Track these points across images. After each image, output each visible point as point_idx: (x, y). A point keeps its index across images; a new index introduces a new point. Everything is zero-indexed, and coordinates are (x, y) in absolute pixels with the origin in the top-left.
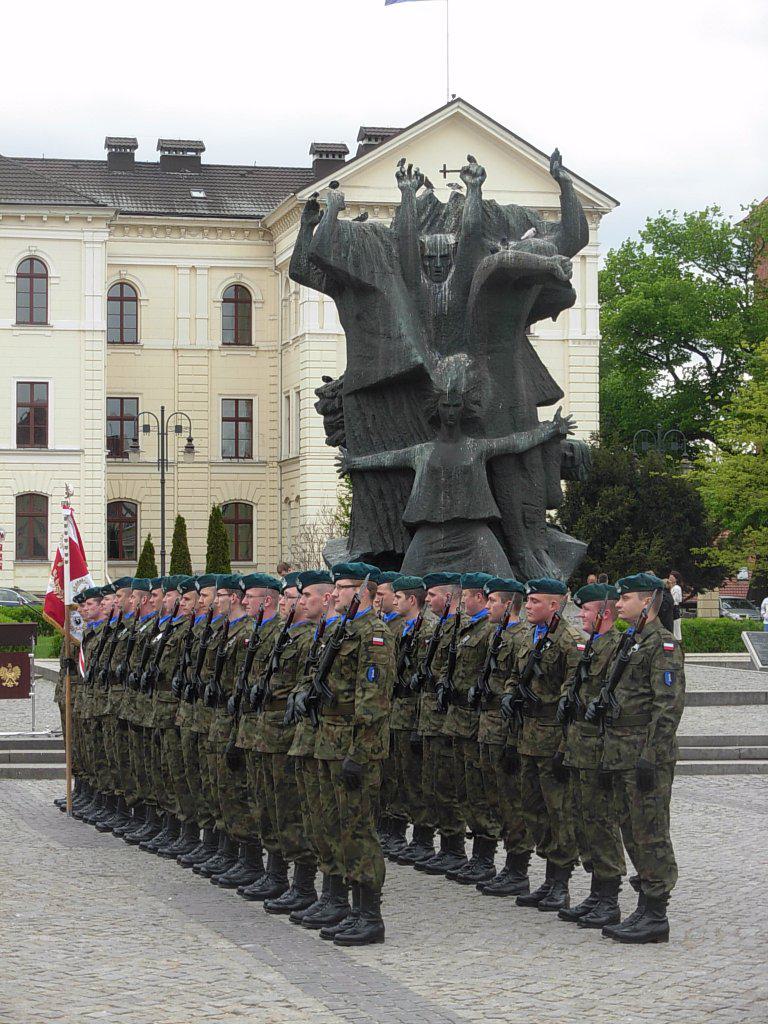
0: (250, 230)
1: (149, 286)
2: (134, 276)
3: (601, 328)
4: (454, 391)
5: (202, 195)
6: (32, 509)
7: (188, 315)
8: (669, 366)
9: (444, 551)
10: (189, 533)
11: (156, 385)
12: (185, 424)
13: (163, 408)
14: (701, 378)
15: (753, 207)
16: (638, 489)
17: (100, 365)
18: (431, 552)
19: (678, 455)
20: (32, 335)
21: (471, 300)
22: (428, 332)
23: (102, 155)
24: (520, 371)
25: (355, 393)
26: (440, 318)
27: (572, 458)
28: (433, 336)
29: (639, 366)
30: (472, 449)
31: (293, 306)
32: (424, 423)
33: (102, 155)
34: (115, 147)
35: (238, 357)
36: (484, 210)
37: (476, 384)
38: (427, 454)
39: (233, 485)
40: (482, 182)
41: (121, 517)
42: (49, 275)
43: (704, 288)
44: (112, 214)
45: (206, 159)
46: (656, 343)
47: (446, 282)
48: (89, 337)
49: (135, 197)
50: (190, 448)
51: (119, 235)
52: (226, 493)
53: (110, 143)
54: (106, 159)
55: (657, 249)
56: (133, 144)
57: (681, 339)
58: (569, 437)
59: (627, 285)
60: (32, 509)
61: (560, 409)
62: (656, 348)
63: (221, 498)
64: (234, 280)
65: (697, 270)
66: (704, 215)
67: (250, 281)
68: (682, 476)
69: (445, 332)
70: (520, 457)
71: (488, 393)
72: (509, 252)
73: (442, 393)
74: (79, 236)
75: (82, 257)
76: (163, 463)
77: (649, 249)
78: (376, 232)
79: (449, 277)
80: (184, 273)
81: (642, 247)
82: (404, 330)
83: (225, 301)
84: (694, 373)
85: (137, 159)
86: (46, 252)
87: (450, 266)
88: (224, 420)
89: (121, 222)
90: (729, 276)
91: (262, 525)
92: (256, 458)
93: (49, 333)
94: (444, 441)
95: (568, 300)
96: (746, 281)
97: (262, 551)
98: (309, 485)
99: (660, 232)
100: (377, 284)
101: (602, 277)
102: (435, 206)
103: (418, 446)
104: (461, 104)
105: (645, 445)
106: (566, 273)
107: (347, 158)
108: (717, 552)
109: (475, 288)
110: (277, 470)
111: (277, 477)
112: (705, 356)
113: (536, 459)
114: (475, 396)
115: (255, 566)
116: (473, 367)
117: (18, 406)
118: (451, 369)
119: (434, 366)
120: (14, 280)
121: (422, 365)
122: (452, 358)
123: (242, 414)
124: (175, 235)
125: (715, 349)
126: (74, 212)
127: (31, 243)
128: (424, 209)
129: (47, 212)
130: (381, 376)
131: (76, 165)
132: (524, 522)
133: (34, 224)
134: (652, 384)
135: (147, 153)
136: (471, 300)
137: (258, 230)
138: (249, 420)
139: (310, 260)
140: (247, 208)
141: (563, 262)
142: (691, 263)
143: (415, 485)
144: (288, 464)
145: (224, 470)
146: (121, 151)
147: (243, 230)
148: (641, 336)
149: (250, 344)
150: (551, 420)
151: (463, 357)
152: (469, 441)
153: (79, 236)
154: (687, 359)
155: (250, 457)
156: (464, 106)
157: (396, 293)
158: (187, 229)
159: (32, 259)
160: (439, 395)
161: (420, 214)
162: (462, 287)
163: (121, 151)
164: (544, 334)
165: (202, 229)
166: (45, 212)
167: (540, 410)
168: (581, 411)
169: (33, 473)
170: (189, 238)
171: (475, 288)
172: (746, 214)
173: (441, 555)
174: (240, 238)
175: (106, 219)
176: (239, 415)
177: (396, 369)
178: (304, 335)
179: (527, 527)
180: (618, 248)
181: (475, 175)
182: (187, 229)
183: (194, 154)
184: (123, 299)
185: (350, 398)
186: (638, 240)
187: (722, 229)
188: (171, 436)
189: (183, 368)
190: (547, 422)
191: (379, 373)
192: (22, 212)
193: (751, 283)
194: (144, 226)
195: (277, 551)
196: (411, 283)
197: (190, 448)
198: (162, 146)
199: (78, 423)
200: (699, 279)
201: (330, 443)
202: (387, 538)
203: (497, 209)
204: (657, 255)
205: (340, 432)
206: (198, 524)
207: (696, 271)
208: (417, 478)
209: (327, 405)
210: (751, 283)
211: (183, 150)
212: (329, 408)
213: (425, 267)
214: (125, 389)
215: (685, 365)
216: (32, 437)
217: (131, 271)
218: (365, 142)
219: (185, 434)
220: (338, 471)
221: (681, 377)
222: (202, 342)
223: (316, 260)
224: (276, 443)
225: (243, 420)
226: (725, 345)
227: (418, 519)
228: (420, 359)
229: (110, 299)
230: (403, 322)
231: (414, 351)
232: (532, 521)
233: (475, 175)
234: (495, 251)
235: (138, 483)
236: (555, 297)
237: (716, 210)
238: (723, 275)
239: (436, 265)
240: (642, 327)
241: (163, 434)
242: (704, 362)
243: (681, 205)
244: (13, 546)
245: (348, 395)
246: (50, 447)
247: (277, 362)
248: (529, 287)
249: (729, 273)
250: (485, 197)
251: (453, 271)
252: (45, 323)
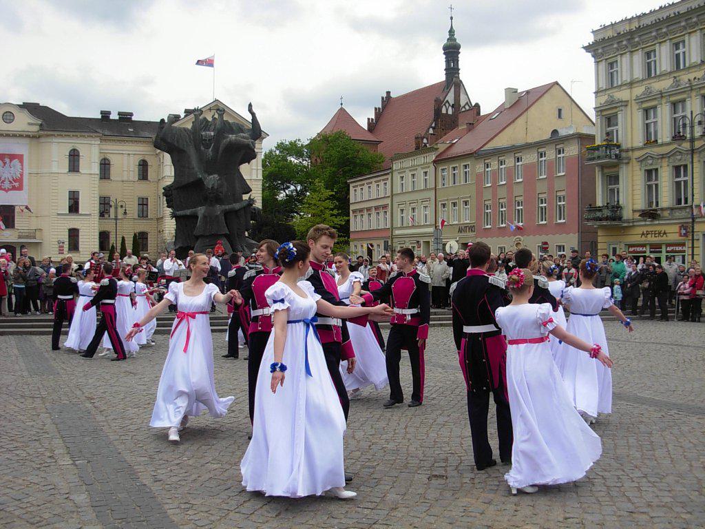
1: (115, 160)
2: (110, 157)
4: (212, 188)
10: (126, 242)
11: (114, 190)
12: (124, 205)
19: (288, 217)
21: (219, 155)
23: (100, 117)
24: (237, 182)
25: (177, 189)
30: (219, 209)
33: (100, 117)
35: (144, 184)
37: (221, 186)
39: (142, 226)
45: (134, 118)
48: (93, 176)
50: (125, 213)
56: (109, 113)
57: (287, 181)
63: (138, 230)
65: (293, 159)
66: (295, 142)
69: (209, 167)
70: (236, 212)
72: (232, 137)
73: (209, 188)
74: (89, 142)
76: (116, 219)
77: (278, 152)
80: (126, 157)
86: (79, 147)
89: (104, 139)
99: (281, 146)
100: (185, 149)
109: (220, 151)
118: (212, 180)
119: (206, 179)
123: (144, 203)
124: (123, 143)
133: (75, 138)
135: (114, 116)
136: (219, 155)
138: (147, 205)
139: (161, 140)
144: (160, 219)
148: (275, 180)
151: (216, 176)
153: (89, 142)
154: (289, 187)
157: (192, 152)
158: (127, 141)
159: (74, 150)
162: (216, 150)
164: (244, 169)
166: (78, 134)
167: (244, 195)
168: (256, 195)
169: (74, 222)
171: (220, 151)
176: (143, 203)
177: (192, 180)
182: (127, 141)
184: (105, 166)
186: (275, 149)
188: (119, 208)
189: (125, 186)
196: (197, 149)
197: (125, 213)
198: (119, 114)
199: (89, 204)
207: (293, 159)
222: (131, 179)
223: (163, 140)
230: (194, 162)
231: (198, 173)
235: (109, 226)
236: (249, 155)
237: (299, 140)
239: (207, 143)
240: (277, 173)
241: (116, 208)
243: (288, 138)
247: (156, 185)
249: (303, 160)
252: (78, 171)
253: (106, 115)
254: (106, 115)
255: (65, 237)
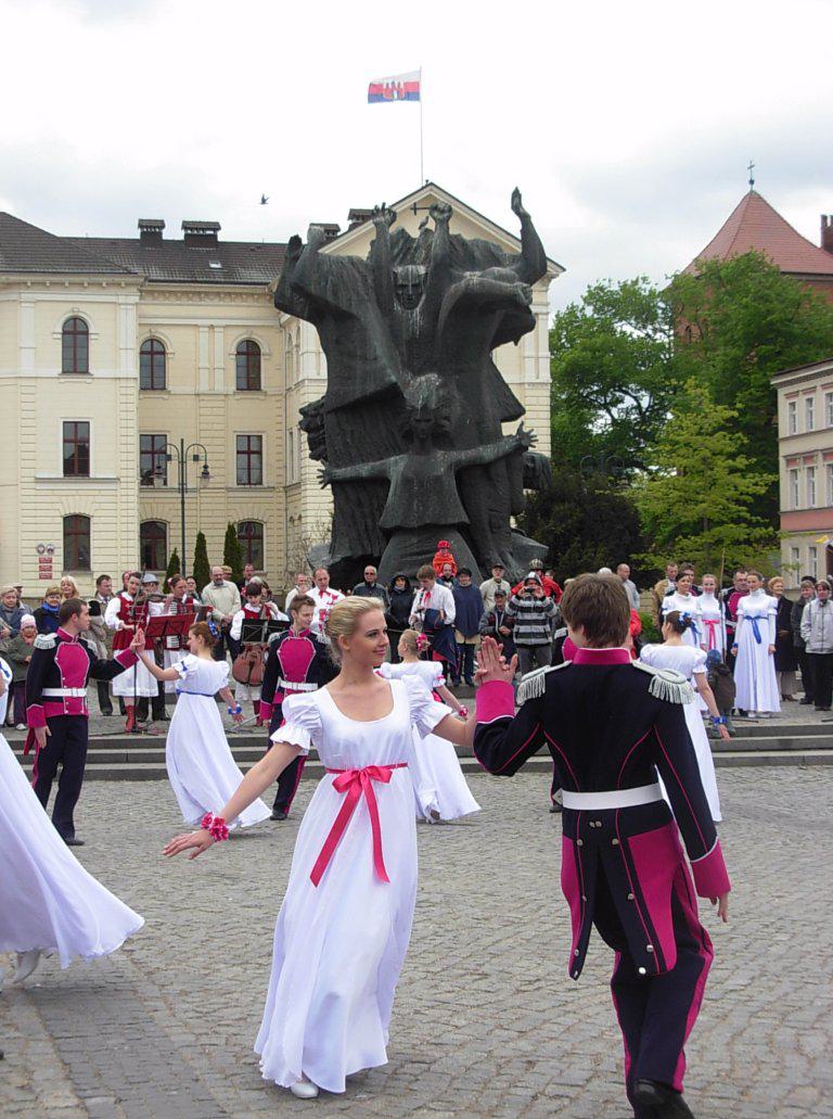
0: (258, 294)
1: (175, 341)
3: (552, 375)
4: (425, 407)
5: (219, 266)
6: (77, 529)
7: (208, 366)
8: (606, 407)
9: (418, 554)
10: (208, 548)
11: (178, 420)
12: (202, 455)
13: (182, 440)
14: (633, 417)
15: (676, 276)
16: (586, 506)
17: (133, 407)
18: (406, 556)
20: (76, 383)
21: (441, 324)
22: (402, 354)
23: (136, 234)
25: (336, 411)
26: (412, 343)
27: (534, 469)
28: (406, 359)
29: (582, 407)
30: (442, 461)
31: (295, 356)
32: (399, 439)
33: (136, 234)
34: (147, 227)
35: (250, 401)
36: (451, 243)
37: (445, 402)
38: (401, 466)
39: (246, 507)
40: (449, 217)
41: (152, 535)
42: (90, 332)
43: (634, 342)
44: (142, 280)
45: (222, 237)
46: (596, 388)
47: (418, 309)
48: (123, 383)
49: (162, 268)
50: (206, 474)
51: (149, 300)
52: (241, 514)
53: (142, 224)
54: (138, 237)
55: (596, 310)
56: (161, 225)
57: (615, 383)
58: (530, 449)
59: (571, 340)
60: (77, 529)
61: (522, 424)
62: (596, 392)
64: (245, 336)
65: (628, 329)
66: (635, 283)
67: (258, 337)
68: (623, 494)
69: (417, 353)
70: (485, 468)
71: (456, 410)
72: (473, 277)
73: (414, 409)
74: (113, 299)
75: (118, 323)
76: (183, 490)
77: (589, 311)
78: (353, 264)
79: (421, 303)
80: (205, 334)
81: (583, 309)
82: (379, 352)
83: (238, 353)
84: (627, 413)
85: (165, 237)
87: (421, 295)
88: (238, 452)
89: (149, 289)
90: (655, 333)
91: (272, 540)
92: (265, 485)
93: (90, 381)
94: (417, 454)
95: (529, 325)
96: (669, 336)
97: (271, 562)
98: (308, 507)
99: (597, 296)
100: (354, 311)
101: (551, 335)
102: (405, 242)
103: (392, 458)
104: (433, 187)
105: (589, 470)
106: (527, 298)
107: (339, 234)
108: (652, 558)
109: (443, 314)
110: (283, 494)
111: (283, 500)
112: (635, 398)
113: (501, 469)
114: (445, 411)
115: (265, 575)
116: (444, 385)
117: (65, 441)
118: (423, 388)
120: (60, 336)
121: (396, 384)
122: (423, 378)
124: (196, 298)
125: (643, 392)
126: (110, 280)
127: (74, 305)
128: (397, 243)
129: (87, 279)
130: (358, 395)
131: (114, 242)
132: (491, 528)
134: (592, 422)
136: (441, 324)
137: (265, 294)
138: (260, 453)
140: (257, 276)
141: (523, 289)
142: (624, 322)
143: (390, 494)
144: (292, 489)
145: (237, 494)
146: (151, 230)
147: (253, 294)
148: (584, 383)
149: (259, 389)
150: (514, 434)
151: (433, 376)
152: (440, 454)
153: (113, 299)
154: (622, 401)
155: (261, 483)
156: (436, 190)
157: (371, 318)
158: (207, 294)
160: (412, 411)
161: (392, 248)
162: (432, 313)
163: (151, 230)
164: (505, 357)
165: (218, 294)
166: (85, 279)
167: (503, 425)
168: (537, 424)
169: (77, 496)
170: (208, 301)
171: (443, 314)
172: (670, 282)
173: (415, 558)
174: (250, 301)
175: (137, 284)
176: (250, 449)
177: (371, 388)
178: (304, 380)
179: (493, 532)
180: (563, 310)
181: (442, 212)
182: (207, 294)
183: (212, 232)
184: (153, 358)
185: (329, 416)
186: (581, 303)
187: (650, 295)
188: (190, 463)
190: (510, 436)
191: (357, 391)
192: (66, 279)
193: (672, 338)
194: (170, 292)
195: (283, 562)
196: (385, 310)
197: (206, 474)
198: (186, 225)
199: (114, 455)
200: (631, 335)
201: (313, 457)
202: (366, 543)
203: (464, 243)
204: (596, 316)
205: (322, 447)
206: (217, 539)
207: (628, 329)
208: (392, 489)
209: (310, 422)
210: (672, 338)
211: (203, 230)
212: (312, 426)
213: (397, 294)
214: (155, 427)
215: (620, 406)
216: (76, 467)
217: (162, 330)
218: (355, 221)
219: (202, 463)
220: (320, 483)
221: (616, 416)
222: (219, 388)
223: (298, 289)
224: (282, 472)
225: (254, 452)
226: (653, 389)
227: (394, 525)
228: (393, 378)
229: (142, 353)
230: (379, 344)
232: (499, 527)
233: (442, 212)
234: (462, 278)
235: (165, 507)
236: (516, 321)
238: (650, 332)
239: (406, 293)
240: (587, 367)
241: (182, 462)
242: (635, 404)
243: (614, 277)
244: (61, 559)
245: (329, 412)
246: (91, 476)
248: (493, 312)
249: (655, 330)
250: (452, 232)
251: (424, 297)
253: (151, 230)
254: (151, 230)
255: (56, 539)
